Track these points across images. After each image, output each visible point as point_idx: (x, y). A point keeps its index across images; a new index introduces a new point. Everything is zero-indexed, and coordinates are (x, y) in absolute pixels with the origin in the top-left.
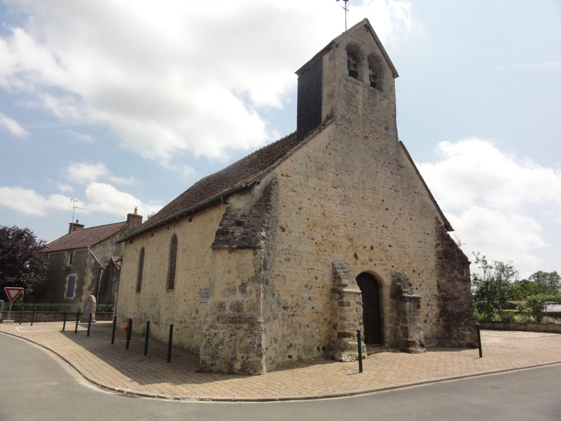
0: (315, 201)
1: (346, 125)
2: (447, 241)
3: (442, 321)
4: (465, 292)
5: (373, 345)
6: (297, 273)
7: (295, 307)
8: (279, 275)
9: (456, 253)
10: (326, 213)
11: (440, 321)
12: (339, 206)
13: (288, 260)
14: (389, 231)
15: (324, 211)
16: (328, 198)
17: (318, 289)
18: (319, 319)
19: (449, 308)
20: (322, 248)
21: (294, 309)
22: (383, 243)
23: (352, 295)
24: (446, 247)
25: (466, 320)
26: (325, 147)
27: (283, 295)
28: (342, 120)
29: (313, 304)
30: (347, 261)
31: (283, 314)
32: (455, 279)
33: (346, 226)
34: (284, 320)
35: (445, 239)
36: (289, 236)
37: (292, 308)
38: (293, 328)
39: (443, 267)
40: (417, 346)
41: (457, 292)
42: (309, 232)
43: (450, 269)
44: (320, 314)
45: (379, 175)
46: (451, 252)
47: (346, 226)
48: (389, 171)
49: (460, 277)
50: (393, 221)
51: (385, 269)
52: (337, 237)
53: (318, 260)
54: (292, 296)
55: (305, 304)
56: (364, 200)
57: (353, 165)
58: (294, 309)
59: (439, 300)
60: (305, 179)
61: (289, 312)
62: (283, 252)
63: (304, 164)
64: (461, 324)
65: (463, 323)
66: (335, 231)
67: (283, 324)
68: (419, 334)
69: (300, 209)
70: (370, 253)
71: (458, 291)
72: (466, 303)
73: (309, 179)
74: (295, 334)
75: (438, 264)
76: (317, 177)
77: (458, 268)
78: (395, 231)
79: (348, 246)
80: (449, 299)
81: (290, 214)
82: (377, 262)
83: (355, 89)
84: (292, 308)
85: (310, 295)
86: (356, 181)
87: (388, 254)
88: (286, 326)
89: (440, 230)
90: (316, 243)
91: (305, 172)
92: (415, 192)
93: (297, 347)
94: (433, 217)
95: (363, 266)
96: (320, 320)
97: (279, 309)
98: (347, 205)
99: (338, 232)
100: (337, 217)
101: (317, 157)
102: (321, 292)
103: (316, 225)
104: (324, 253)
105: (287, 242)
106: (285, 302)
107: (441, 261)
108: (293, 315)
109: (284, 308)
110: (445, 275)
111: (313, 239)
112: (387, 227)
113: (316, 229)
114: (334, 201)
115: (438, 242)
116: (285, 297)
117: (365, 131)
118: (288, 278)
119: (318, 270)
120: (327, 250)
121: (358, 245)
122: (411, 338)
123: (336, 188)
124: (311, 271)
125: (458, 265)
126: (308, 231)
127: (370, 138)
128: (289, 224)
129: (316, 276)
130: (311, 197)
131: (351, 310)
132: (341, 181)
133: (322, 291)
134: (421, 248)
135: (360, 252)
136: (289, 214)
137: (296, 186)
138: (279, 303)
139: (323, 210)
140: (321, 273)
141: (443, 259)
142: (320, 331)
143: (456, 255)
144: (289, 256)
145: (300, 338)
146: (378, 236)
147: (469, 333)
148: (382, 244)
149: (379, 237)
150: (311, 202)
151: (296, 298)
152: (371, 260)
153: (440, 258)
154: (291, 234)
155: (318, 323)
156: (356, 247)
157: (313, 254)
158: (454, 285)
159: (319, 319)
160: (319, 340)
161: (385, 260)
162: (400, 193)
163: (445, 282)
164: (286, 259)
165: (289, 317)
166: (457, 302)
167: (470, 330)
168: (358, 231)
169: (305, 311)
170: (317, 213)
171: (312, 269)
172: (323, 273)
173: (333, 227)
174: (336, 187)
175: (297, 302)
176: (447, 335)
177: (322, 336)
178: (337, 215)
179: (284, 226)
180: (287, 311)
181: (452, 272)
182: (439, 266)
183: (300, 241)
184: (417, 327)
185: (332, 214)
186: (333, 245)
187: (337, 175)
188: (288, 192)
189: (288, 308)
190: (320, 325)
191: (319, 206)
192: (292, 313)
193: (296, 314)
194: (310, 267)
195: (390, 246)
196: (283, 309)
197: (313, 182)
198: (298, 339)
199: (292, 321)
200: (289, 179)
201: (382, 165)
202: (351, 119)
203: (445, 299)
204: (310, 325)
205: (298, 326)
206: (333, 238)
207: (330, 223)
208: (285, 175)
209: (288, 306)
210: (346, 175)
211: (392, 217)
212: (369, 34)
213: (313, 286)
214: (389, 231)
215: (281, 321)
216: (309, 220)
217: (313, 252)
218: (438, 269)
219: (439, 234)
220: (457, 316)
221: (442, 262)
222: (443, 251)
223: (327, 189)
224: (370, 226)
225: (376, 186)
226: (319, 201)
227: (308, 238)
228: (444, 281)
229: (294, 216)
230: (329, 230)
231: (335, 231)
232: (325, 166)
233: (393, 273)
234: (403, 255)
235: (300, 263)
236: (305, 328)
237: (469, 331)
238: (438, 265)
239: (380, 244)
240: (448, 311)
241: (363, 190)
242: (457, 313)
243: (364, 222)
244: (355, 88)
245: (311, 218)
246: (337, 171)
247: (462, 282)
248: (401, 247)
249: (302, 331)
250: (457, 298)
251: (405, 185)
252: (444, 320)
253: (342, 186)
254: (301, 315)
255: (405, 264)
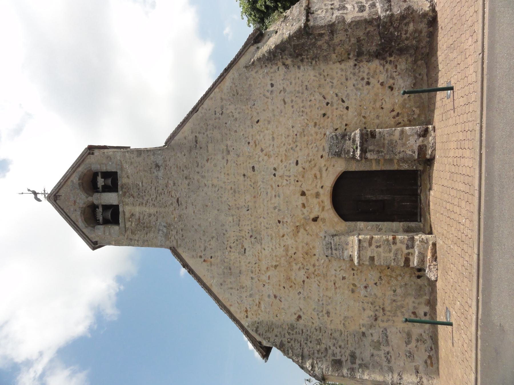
0: (264, 278)
1: (174, 232)
2: (276, 55)
3: (392, 59)
4: (350, 30)
5: (419, 184)
6: (340, 303)
7: (375, 307)
8: (344, 324)
9: (293, 43)
10: (274, 264)
11: (391, 61)
12: (263, 246)
13: (328, 313)
14: (279, 165)
15: (272, 266)
16: (258, 261)
17: (356, 276)
18: (387, 276)
19: (373, 48)
20: (312, 269)
21: (377, 308)
22: (295, 176)
23: (362, 252)
24: (285, 55)
25: (392, 29)
26: (204, 263)
27: (363, 320)
28: (171, 238)
29: (371, 283)
30: (322, 234)
31: (383, 321)
32: (330, 43)
33: (283, 236)
34: (388, 320)
35: (275, 56)
36: (305, 311)
37: (377, 310)
38: (396, 310)
39: (315, 58)
40: (425, 143)
41: (350, 41)
42: (297, 286)
43: (317, 50)
44: (382, 275)
45: (215, 182)
46: (292, 50)
47: (283, 236)
48: (208, 165)
49: (327, 38)
50: (266, 158)
51: (326, 170)
52: (297, 249)
53: (325, 276)
54: (364, 310)
55: (371, 295)
56: (249, 208)
57: (214, 224)
58: (377, 308)
59: (361, 61)
60: (244, 290)
61: (380, 314)
62: (321, 318)
63: (231, 291)
64: (398, 36)
65: (396, 33)
66: (291, 252)
67: (392, 322)
68: (410, 135)
69: (275, 297)
70: (309, 197)
71: (348, 40)
72: (366, 28)
73: (244, 285)
74: (403, 307)
75: (310, 64)
76: (239, 276)
77: (314, 40)
78: (278, 154)
79: (305, 232)
80: (360, 48)
81: (283, 308)
82: (319, 185)
83: (131, 217)
84: (377, 310)
85: (362, 287)
86: (230, 219)
87: (307, 165)
88: (394, 318)
89: (262, 62)
90: (308, 278)
91: (238, 290)
92: (222, 114)
93: (416, 305)
94: (247, 75)
95: (326, 208)
96: (389, 274)
97: (377, 326)
98: (260, 234)
99: (292, 248)
100: (276, 248)
101: (218, 274)
102: (359, 271)
103: (288, 278)
104: (316, 267)
105: (311, 314)
106: (371, 319)
107: (306, 60)
108: (383, 309)
109: (376, 320)
110: (325, 56)
111: (304, 281)
112: (275, 169)
113: (293, 278)
114: (259, 252)
115: (280, 64)
116: (365, 318)
117: (172, 204)
118: (346, 314)
119: (335, 276)
120: (312, 263)
121: (303, 216)
122: (414, 153)
123: (245, 249)
124: (337, 285)
125: (309, 40)
126: (297, 288)
127: (177, 197)
128: (293, 310)
129: (341, 279)
130: (261, 283)
131: (379, 255)
132: (236, 242)
133: (357, 270)
134: (292, 101)
135: (310, 213)
136: (283, 311)
137: (254, 302)
138: (371, 326)
139: (271, 268)
140: (338, 272)
141: (303, 58)
142: (401, 275)
143: (294, 43)
144: (325, 312)
145: (407, 300)
146: (287, 184)
147: (411, 25)
148: (297, 176)
149: (288, 183)
150: (266, 282)
151: (366, 305)
152: (317, 195)
153: (302, 60)
154: (302, 308)
155: (391, 277)
156: (305, 218)
157: (320, 282)
158: (339, 44)
159: (387, 276)
160: (410, 277)
161: (316, 171)
162: (229, 143)
163: (336, 54)
164: (328, 316)
165: (385, 314)
166: (364, 39)
167: (407, 24)
168: (286, 218)
169: (379, 294)
170: (276, 276)
171: (335, 284)
172: (338, 270)
173: (287, 255)
174: (244, 249)
175: (370, 303)
176: (412, 51)
177: (406, 272)
178: (274, 248)
179: (296, 316)
180: (379, 316)
181: (320, 47)
182: (314, 62)
183: (308, 297)
184: (400, 139)
185: (274, 255)
186: (307, 254)
187: (231, 248)
188: (262, 311)
189: (376, 315)
190: (394, 275)
191: (269, 273)
192: (381, 311)
193: (382, 307)
194: (333, 285)
195: (297, 163)
196: (377, 321)
197: (246, 281)
198: (407, 303)
199: (389, 311)
200: (249, 309)
201: (203, 177)
202: (165, 224)
203: (360, 54)
204: (393, 288)
205: (394, 303)
206: (299, 254)
207: (284, 258)
208: (246, 315)
209: (374, 315)
210: (228, 235)
211: (261, 159)
212: (61, 192)
213: (353, 282)
214: (279, 165)
215: (390, 323)
216: (285, 286)
217: (317, 282)
218: (318, 64)
219: (268, 63)
220: (385, 40)
221: (307, 58)
222: (292, 58)
223: (249, 263)
224: (277, 198)
225: (229, 187)
226: (263, 272)
227: (303, 288)
228: (334, 56)
229: (284, 305)
230: (292, 260)
231: (291, 252)
232: (226, 264)
233: (330, 157)
234: (306, 137)
235: (330, 298)
236: (396, 295)
237: (408, 25)
238: (311, 63)
239: (297, 181)
240: (377, 50)
241: (238, 208)
242: (381, 40)
243: (275, 208)
244: (129, 219)
245: (283, 285)
246: (226, 248)
247: (335, 36)
248: (296, 141)
249: (399, 298)
250: (359, 40)
251: (217, 134)
252: (391, 55)
253: (241, 241)
254: (383, 300)
255: (316, 133)
